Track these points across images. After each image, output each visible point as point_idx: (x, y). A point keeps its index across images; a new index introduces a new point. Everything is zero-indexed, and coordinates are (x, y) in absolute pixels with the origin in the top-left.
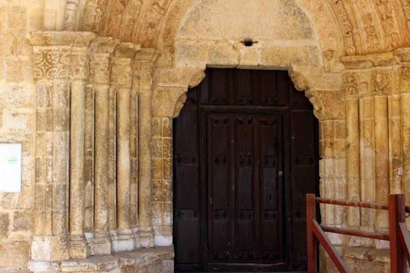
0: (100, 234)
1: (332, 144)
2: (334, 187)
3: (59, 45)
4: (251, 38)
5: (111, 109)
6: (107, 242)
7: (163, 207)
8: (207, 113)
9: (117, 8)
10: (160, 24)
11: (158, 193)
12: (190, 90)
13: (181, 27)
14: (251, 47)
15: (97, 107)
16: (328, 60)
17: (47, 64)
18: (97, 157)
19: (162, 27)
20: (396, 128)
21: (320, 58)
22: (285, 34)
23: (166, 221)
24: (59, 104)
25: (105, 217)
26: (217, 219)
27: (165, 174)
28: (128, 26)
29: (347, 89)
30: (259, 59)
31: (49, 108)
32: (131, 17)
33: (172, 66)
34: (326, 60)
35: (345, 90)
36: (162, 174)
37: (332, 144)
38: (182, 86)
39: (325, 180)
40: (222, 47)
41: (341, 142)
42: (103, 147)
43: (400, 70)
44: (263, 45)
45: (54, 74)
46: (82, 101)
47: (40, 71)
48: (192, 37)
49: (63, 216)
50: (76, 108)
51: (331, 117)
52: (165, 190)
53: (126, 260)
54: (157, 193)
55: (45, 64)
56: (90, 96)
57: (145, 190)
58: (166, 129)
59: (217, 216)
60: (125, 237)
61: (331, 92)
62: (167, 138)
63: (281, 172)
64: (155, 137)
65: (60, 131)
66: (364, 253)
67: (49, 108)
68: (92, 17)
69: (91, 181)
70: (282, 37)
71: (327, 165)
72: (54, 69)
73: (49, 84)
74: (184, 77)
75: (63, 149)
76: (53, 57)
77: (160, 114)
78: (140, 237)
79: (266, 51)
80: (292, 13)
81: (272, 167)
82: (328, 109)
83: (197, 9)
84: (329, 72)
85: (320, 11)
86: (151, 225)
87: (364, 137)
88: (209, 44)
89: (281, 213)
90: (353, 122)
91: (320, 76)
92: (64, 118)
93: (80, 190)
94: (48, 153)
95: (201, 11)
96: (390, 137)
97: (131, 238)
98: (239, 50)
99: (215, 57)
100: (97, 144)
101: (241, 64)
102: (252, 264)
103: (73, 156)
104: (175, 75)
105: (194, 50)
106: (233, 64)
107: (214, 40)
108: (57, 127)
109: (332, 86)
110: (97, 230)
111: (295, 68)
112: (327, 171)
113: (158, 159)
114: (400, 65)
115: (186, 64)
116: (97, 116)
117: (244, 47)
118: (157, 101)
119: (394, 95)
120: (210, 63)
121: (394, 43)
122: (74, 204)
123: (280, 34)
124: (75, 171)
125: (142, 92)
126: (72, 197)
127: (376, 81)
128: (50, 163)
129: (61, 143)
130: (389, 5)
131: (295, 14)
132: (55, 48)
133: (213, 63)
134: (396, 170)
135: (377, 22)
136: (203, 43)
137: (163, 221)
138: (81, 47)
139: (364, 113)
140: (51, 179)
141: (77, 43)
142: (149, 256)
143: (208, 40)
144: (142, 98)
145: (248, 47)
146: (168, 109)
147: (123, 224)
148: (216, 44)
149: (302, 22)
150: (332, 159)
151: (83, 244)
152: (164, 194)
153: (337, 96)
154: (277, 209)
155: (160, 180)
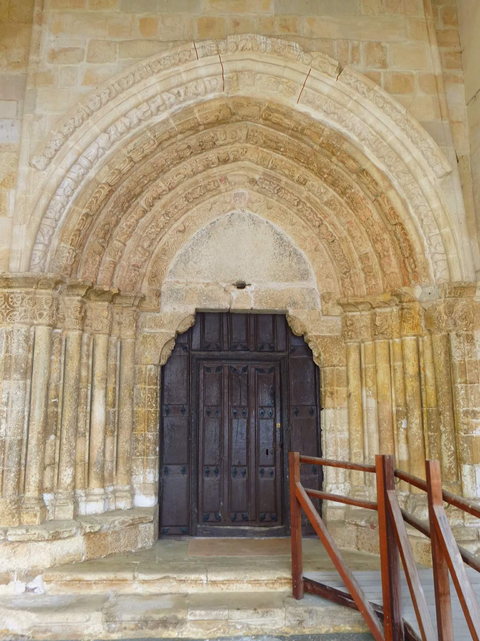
0: (63, 494)
1: (332, 393)
2: (335, 441)
3: (21, 287)
5: (84, 356)
6: (70, 504)
7: (145, 463)
8: (199, 359)
10: (146, 266)
11: (141, 447)
12: (179, 335)
13: (169, 270)
14: (244, 290)
15: (67, 353)
16: (326, 303)
17: (8, 307)
18: (65, 408)
19: (148, 269)
20: (399, 375)
21: (318, 300)
22: (280, 276)
23: (148, 478)
24: (18, 350)
25: (70, 476)
26: (208, 476)
27: (148, 426)
28: (107, 268)
29: (346, 333)
30: (252, 302)
31: (8, 355)
32: (112, 259)
33: (158, 310)
34: (324, 303)
35: (344, 334)
36: (146, 427)
37: (332, 393)
39: (326, 433)
40: (212, 291)
41: (343, 391)
42: (72, 397)
43: (400, 312)
44: (256, 288)
45: (15, 317)
46: (45, 347)
48: (180, 280)
49: (15, 476)
50: (38, 354)
51: (330, 364)
52: (148, 444)
53: (89, 525)
54: (140, 448)
55: (6, 307)
56: (58, 342)
57: (124, 444)
58: (151, 377)
59: (208, 473)
60: (95, 498)
61: (330, 337)
62: (152, 387)
64: (139, 386)
65: (18, 380)
66: (366, 519)
67: (8, 355)
68: (64, 259)
69: (56, 435)
70: (277, 279)
71: (328, 416)
72: (15, 313)
73: (9, 328)
74: (171, 322)
75: (20, 399)
76: (15, 300)
77: (144, 361)
78: (116, 497)
79: (260, 293)
80: (288, 254)
81: (268, 419)
83: (187, 251)
84: (327, 315)
85: (317, 251)
86: (130, 483)
87: (366, 385)
88: (199, 286)
89: (279, 469)
90: (353, 369)
91: (318, 320)
92: (23, 365)
93: (38, 445)
94: (2, 403)
95: (190, 252)
96: (393, 385)
97: (101, 498)
99: (205, 301)
100: (65, 394)
101: (233, 308)
102: (247, 528)
106: (224, 308)
107: (204, 283)
108: (15, 376)
109: (332, 331)
110: (60, 491)
111: (291, 312)
112: (328, 423)
113: (141, 410)
115: (174, 309)
116: (67, 363)
117: (236, 290)
118: (142, 348)
119: (395, 339)
120: (199, 307)
121: (392, 283)
123: (275, 276)
124: (34, 425)
125: (124, 337)
126: (29, 453)
127: (375, 324)
128: (5, 415)
129: (18, 393)
130: (385, 243)
131: (290, 255)
132: (18, 290)
133: (202, 307)
134: (400, 422)
135: (374, 261)
136: (192, 286)
137: (145, 478)
138: (46, 289)
139: (365, 360)
140: (4, 433)
141: (41, 285)
142: (120, 520)
143: (198, 283)
144: (124, 345)
145: (240, 290)
146: (152, 357)
147: (94, 483)
150: (332, 410)
151: (37, 508)
152: (147, 449)
153: (335, 341)
154: (274, 465)
155: (142, 432)
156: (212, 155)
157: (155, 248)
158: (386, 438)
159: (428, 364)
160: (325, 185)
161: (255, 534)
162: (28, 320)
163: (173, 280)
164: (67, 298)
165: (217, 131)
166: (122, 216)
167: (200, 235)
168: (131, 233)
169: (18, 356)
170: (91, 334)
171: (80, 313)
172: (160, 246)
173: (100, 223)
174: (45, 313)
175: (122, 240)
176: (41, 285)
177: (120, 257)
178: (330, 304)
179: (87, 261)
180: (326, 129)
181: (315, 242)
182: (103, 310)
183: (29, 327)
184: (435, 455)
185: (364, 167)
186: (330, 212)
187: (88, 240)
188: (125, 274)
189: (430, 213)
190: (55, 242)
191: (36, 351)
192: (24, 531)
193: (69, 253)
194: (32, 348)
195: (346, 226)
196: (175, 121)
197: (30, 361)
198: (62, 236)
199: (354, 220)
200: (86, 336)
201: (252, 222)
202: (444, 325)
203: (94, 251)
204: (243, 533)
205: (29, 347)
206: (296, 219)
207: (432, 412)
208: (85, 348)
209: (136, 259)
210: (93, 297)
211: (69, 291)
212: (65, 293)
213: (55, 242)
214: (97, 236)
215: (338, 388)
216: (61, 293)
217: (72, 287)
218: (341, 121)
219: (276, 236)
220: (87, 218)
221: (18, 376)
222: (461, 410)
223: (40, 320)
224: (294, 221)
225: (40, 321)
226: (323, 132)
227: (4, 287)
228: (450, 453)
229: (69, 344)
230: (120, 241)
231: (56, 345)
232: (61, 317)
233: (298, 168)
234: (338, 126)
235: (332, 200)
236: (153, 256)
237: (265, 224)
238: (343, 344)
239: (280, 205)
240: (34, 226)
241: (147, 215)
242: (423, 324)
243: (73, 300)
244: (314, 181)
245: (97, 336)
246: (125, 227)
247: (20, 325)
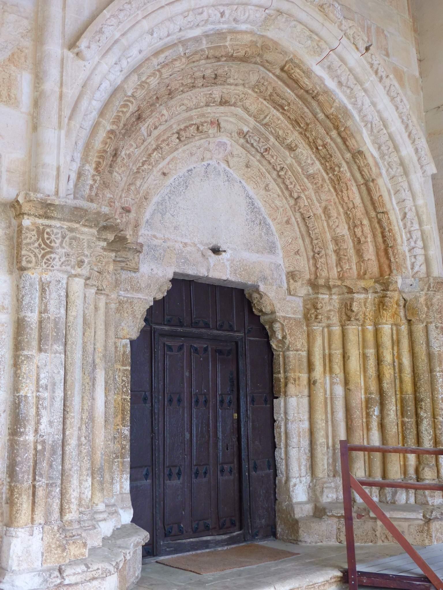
3: (64, 220)
4: (219, 245)
9: (105, 180)
13: (145, 219)
14: (220, 257)
17: (43, 246)
21: (284, 278)
30: (228, 272)
34: (292, 281)
38: (145, 299)
45: (54, 262)
47: (32, 255)
48: (158, 235)
55: (40, 245)
57: (109, 443)
63: (236, 415)
70: (249, 249)
72: (53, 256)
74: (149, 286)
76: (53, 237)
79: (234, 262)
80: (258, 221)
82: (293, 338)
91: (284, 299)
98: (208, 259)
99: (184, 263)
102: (209, 538)
103: (69, 393)
104: (138, 282)
105: (161, 251)
106: (201, 275)
107: (182, 243)
111: (262, 288)
114: (380, 295)
115: (152, 270)
117: (212, 255)
120: (177, 270)
122: (70, 470)
124: (73, 417)
131: (260, 223)
132: (57, 224)
134: (372, 410)
138: (91, 227)
141: (87, 220)
143: (176, 241)
148: (183, 247)
149: (267, 234)
156: (217, 92)
158: (358, 426)
159: (405, 353)
160: (313, 156)
161: (219, 543)
163: (150, 233)
165: (232, 67)
167: (177, 183)
178: (299, 283)
180: (337, 101)
181: (288, 214)
182: (107, 263)
184: (411, 441)
185: (361, 149)
186: (309, 185)
189: (414, 208)
192: (84, 568)
195: (324, 204)
196: (207, 43)
199: (334, 199)
201: (226, 179)
202: (424, 316)
204: (206, 545)
206: (273, 185)
207: (409, 399)
215: (300, 375)
218: (352, 96)
219: (248, 200)
222: (440, 397)
223: (79, 270)
224: (270, 187)
225: (79, 271)
226: (334, 102)
227: (40, 216)
228: (430, 438)
233: (292, 131)
234: (346, 101)
235: (317, 174)
237: (239, 183)
238: (305, 328)
239: (260, 165)
241: (185, 242)
242: (402, 314)
244: (305, 151)
246: (124, 157)
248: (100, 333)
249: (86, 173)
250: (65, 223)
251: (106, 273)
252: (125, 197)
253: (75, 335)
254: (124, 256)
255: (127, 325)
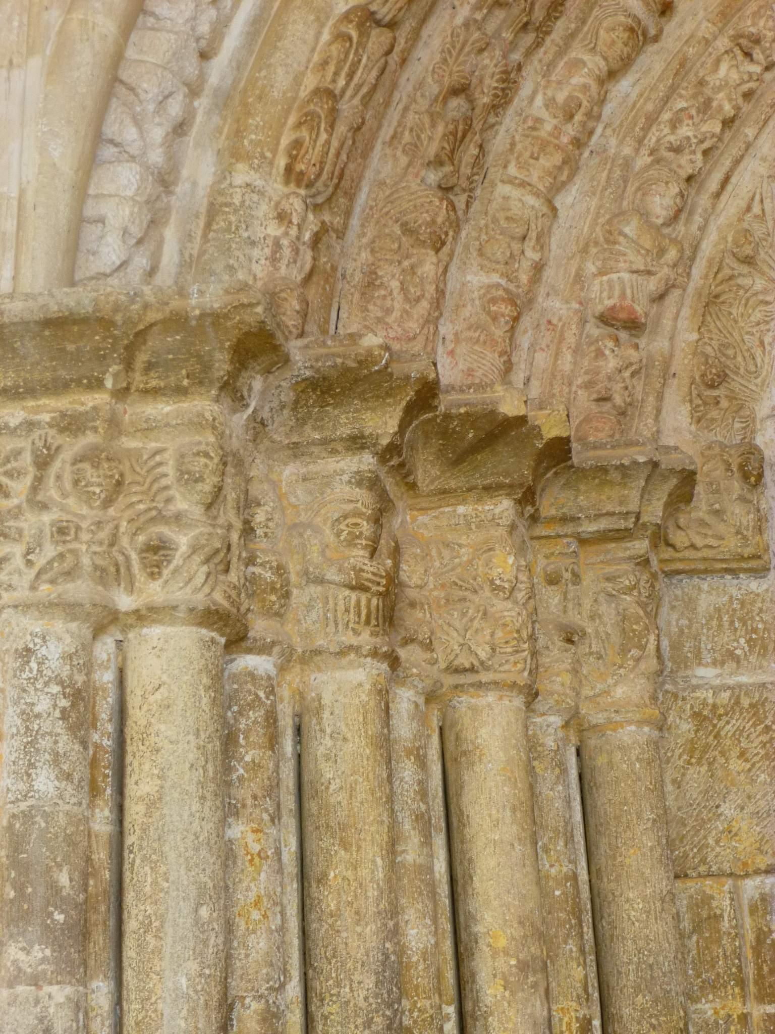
3: (31, 392)
15: (312, 806)
28: (477, 327)
32: (495, 278)
50: (153, 804)
56: (258, 735)
65: (35, 981)
68: (256, 253)
77: (722, 855)
92: (64, 879)
116: (314, 872)
118: (696, 776)
125: (598, 718)
138: (180, 392)
141: (149, 367)
157: (703, 229)
162: (80, 589)
164: (289, 471)
166: (529, 53)
168: (578, 143)
169: (28, 817)
170: (431, 697)
171: (373, 552)
172: (722, 220)
173: (421, 85)
174: (183, 541)
175: (534, 180)
176: (149, 367)
177: (539, 268)
179: (371, 282)
183: (87, 633)
187: (369, 174)
188: (566, 361)
190: (200, 169)
191: (140, 786)
193: (282, 217)
194: (111, 773)
197: (101, 855)
198: (238, 134)
200: (405, 699)
203: (407, 230)
205: (94, 764)
208: (407, 771)
209: (620, 283)
210: (427, 470)
211: (301, 422)
212: (278, 433)
213: (200, 169)
214: (413, 149)
216: (258, 426)
217: (330, 388)
220: (364, 34)
221: (39, 952)
223: (155, 586)
225: (154, 591)
229: (320, 746)
230: (523, 184)
231: (250, 753)
232: (268, 575)
236: (698, 271)
240: (86, 66)
243: (327, 481)
245: (464, 701)
247: (33, 624)
248: (492, 863)
249: (237, 201)
250: (44, 401)
251: (487, 593)
252: (601, 273)
253: (155, 883)
254: (609, 508)
255: (750, 808)
